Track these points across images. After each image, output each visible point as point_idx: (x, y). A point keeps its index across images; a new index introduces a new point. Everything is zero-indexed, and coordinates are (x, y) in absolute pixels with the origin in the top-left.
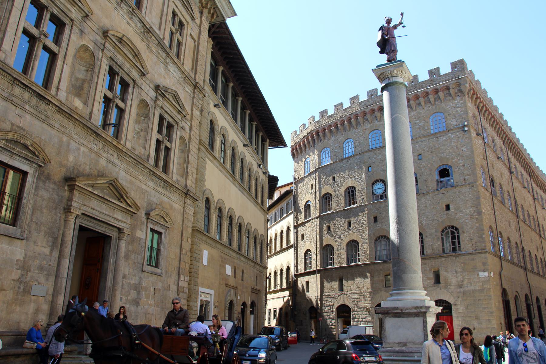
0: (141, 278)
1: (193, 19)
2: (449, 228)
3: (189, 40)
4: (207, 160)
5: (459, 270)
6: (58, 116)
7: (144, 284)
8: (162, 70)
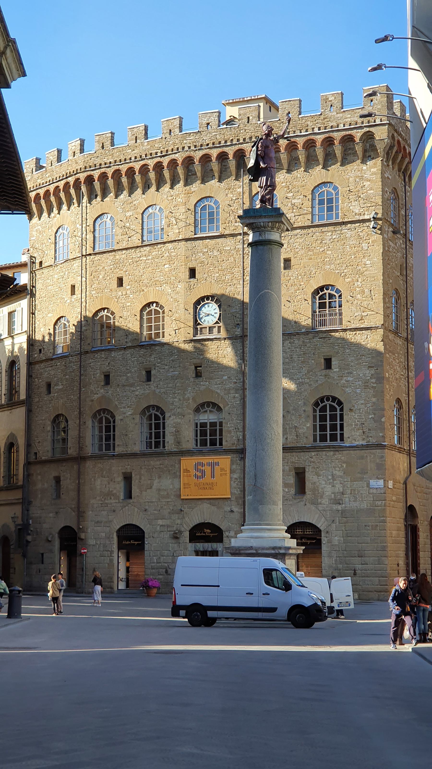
2: (328, 400)
5: (338, 473)
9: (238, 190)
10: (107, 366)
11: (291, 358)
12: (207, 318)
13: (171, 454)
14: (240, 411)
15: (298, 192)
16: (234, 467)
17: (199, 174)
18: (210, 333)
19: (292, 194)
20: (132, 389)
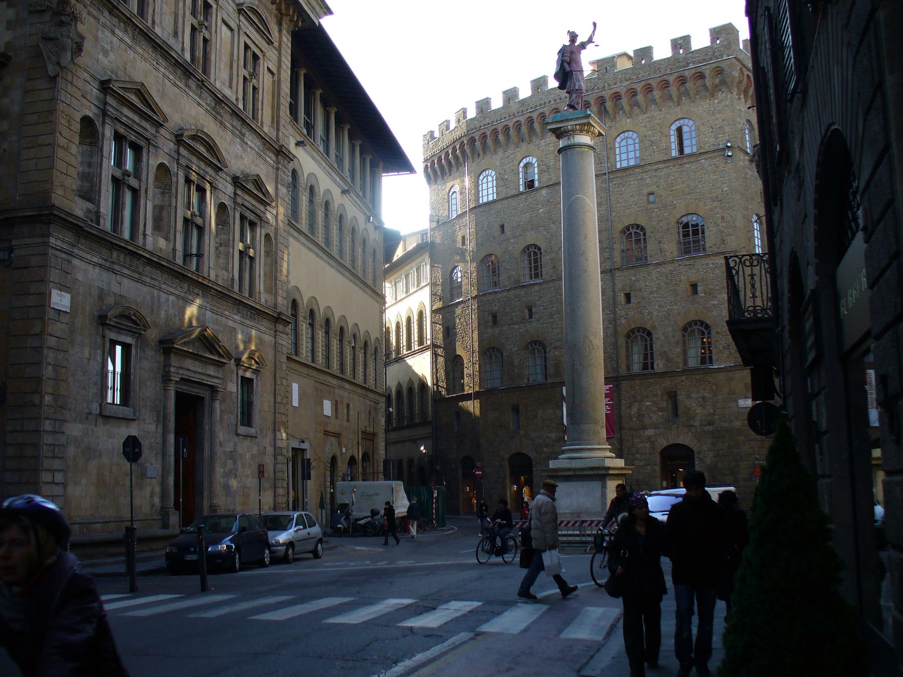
0: (235, 445)
1: (270, 42)
2: (696, 324)
3: (268, 76)
4: (291, 240)
6: (148, 268)
7: (240, 450)
8: (238, 148)
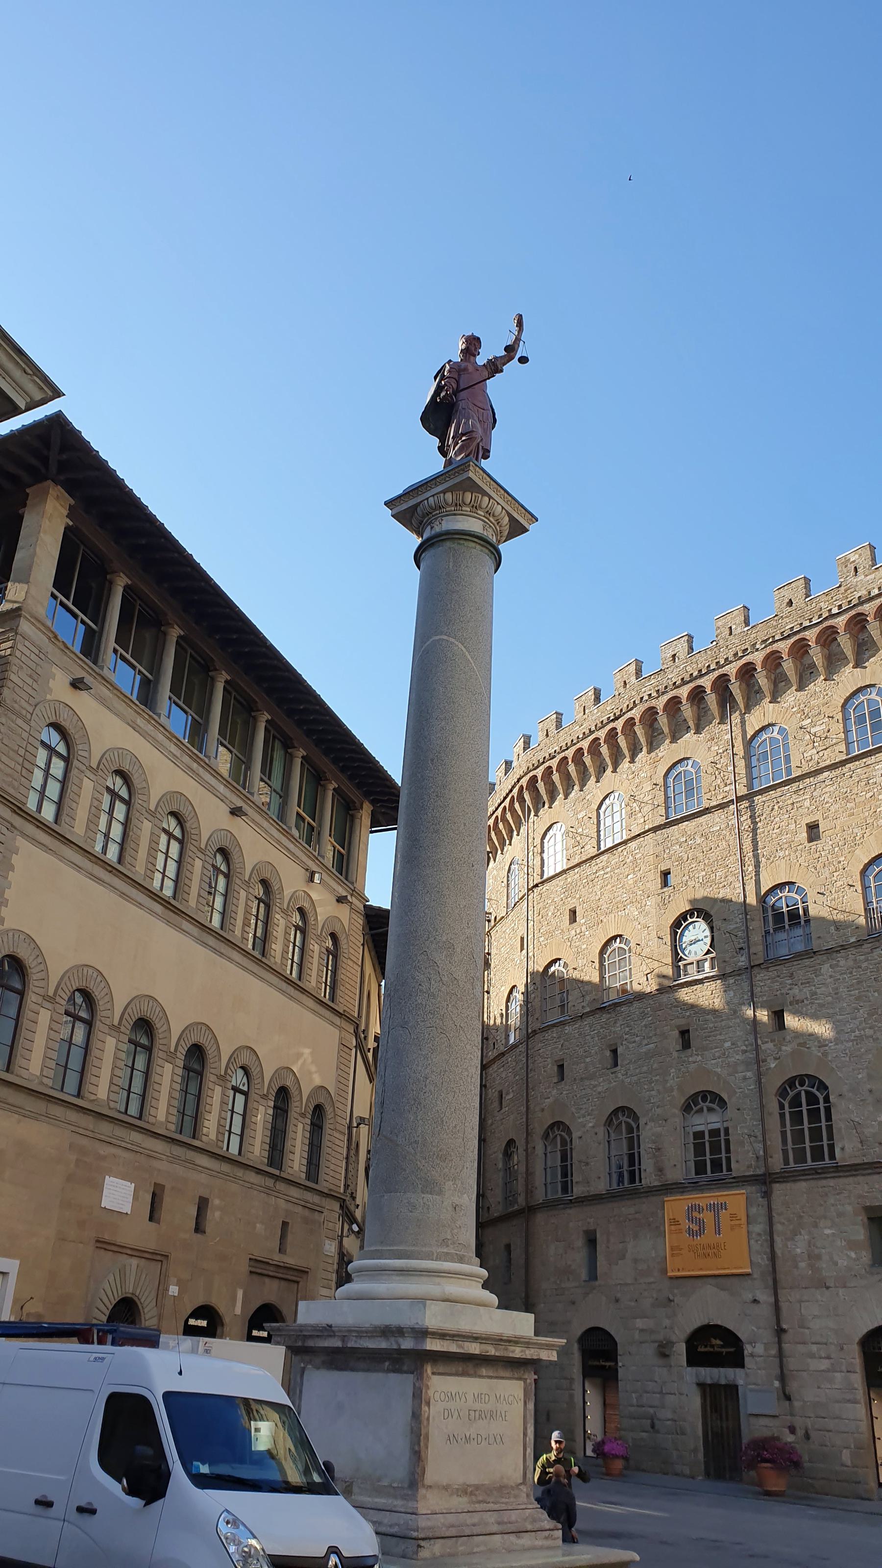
4: (20, 842)
9: (726, 737)
10: (560, 1050)
11: (836, 994)
12: (693, 948)
13: (652, 1191)
14: (756, 1105)
15: (820, 714)
16: (753, 1210)
17: (666, 730)
18: (699, 972)
19: (810, 720)
20: (593, 1083)
